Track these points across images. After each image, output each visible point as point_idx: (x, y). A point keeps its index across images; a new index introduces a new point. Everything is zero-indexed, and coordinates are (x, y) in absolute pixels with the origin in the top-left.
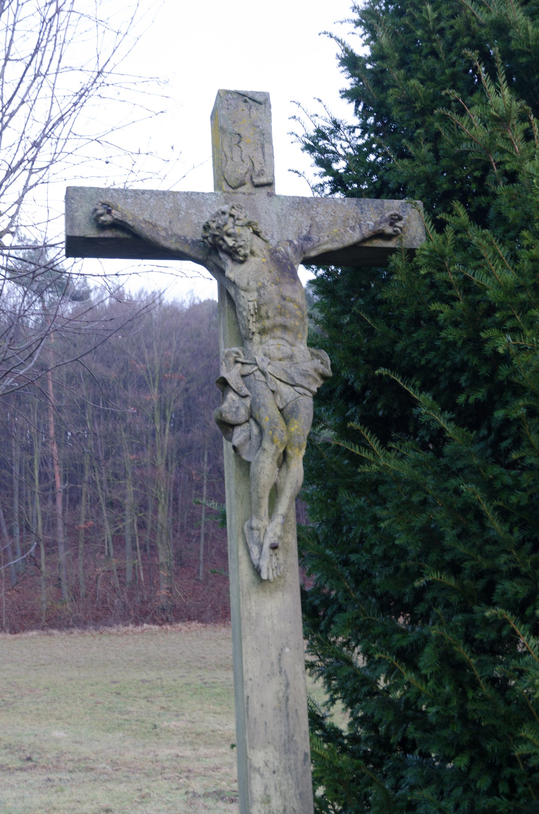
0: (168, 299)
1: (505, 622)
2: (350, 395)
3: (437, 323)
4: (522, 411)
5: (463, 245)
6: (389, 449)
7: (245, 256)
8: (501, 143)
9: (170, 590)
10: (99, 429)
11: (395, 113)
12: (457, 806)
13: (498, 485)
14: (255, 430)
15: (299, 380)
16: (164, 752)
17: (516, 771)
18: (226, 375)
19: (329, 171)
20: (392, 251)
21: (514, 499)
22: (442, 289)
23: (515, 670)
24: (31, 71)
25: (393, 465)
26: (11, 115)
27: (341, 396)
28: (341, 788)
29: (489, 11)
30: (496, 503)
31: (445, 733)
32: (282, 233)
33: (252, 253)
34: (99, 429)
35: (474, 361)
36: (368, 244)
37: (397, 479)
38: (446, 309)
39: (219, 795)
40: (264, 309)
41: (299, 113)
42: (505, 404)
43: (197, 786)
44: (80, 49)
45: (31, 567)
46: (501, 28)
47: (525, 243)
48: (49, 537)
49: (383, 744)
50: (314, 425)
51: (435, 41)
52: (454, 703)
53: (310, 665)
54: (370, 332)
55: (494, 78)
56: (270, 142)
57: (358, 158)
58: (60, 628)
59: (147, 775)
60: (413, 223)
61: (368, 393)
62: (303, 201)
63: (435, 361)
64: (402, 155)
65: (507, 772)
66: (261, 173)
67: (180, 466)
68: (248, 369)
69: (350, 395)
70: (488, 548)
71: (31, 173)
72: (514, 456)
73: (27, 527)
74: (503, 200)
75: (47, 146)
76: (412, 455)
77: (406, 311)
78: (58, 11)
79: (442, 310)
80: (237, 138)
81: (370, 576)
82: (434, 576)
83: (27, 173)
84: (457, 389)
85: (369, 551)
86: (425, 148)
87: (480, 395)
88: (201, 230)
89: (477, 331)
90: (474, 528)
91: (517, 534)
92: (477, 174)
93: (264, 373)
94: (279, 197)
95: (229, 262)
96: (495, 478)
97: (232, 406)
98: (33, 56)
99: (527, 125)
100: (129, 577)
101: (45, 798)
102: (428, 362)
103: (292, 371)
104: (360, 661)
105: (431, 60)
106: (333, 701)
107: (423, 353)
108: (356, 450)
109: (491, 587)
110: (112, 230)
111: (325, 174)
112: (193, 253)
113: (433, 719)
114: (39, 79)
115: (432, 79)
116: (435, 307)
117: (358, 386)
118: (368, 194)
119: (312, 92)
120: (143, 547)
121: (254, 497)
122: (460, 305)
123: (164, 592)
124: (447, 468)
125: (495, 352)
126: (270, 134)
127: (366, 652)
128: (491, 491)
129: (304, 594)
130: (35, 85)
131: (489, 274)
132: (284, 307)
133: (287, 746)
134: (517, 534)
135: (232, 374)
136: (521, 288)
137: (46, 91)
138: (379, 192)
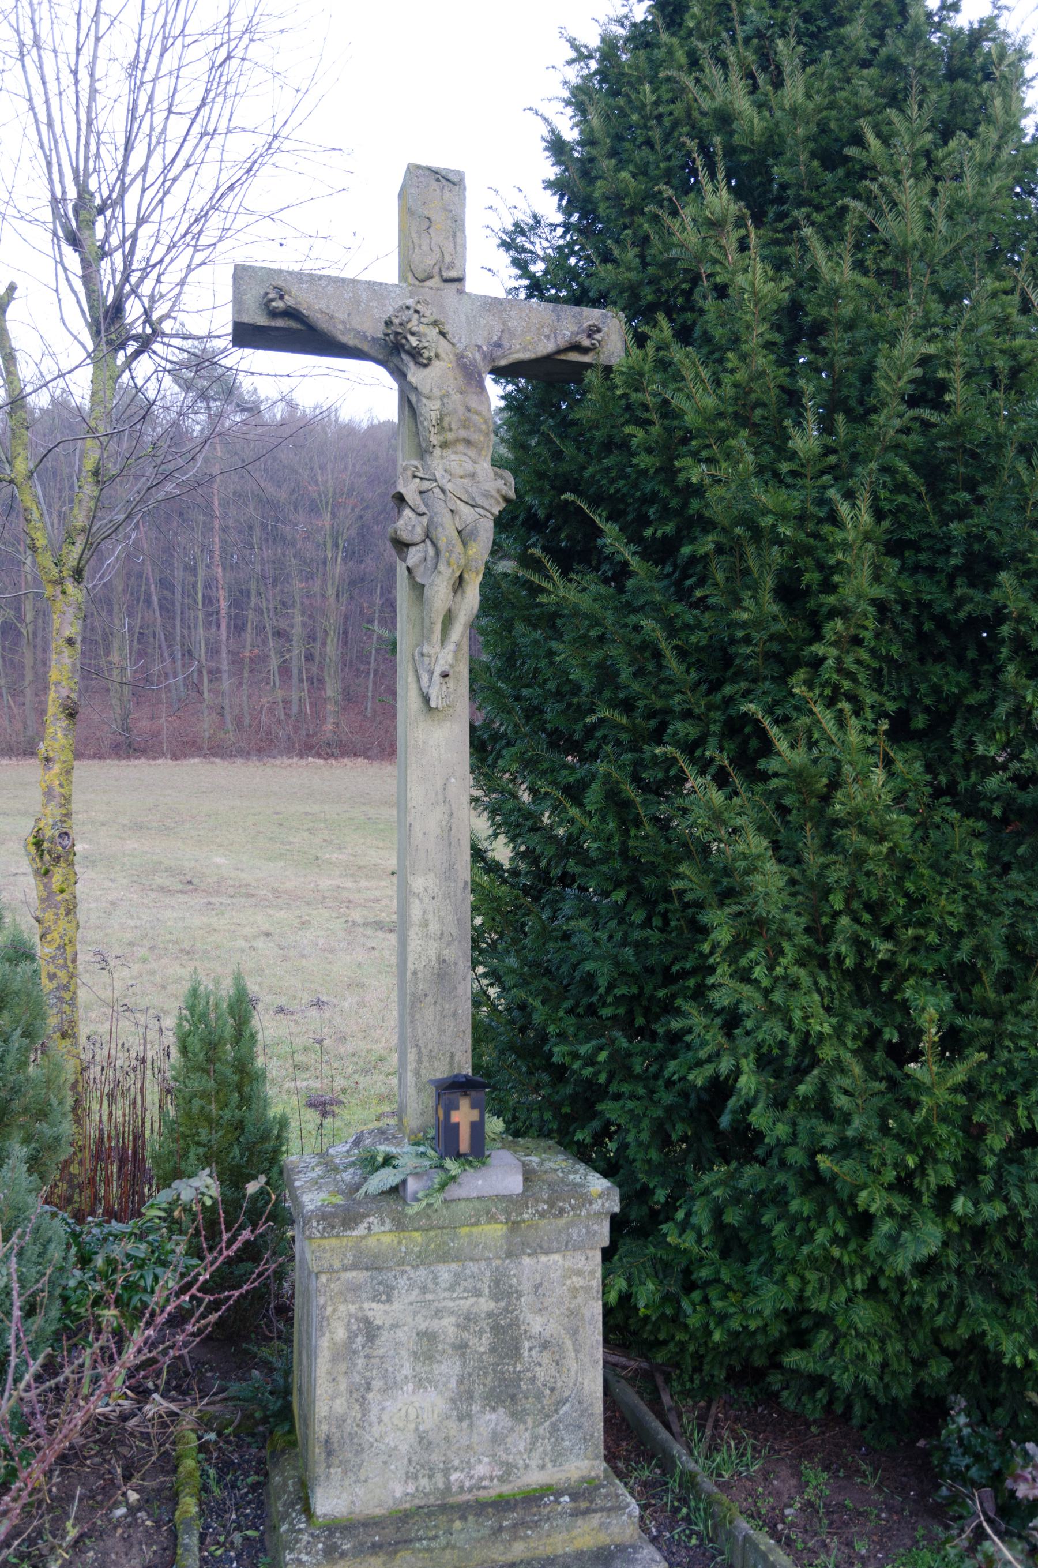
0: (345, 416)
1: (675, 760)
2: (533, 524)
3: (629, 448)
4: (712, 546)
5: (663, 365)
6: (570, 580)
7: (430, 359)
8: (713, 252)
9: (337, 725)
10: (267, 553)
11: (602, 210)
12: (611, 937)
13: (678, 623)
14: (431, 552)
15: (480, 500)
16: (325, 883)
17: (670, 906)
18: (403, 491)
19: (525, 273)
20: (588, 366)
21: (693, 639)
22: (638, 413)
23: (679, 809)
24: (197, 129)
25: (573, 596)
26: (175, 180)
27: (523, 524)
28: (498, 918)
29: (713, 98)
30: (675, 642)
31: (604, 868)
32: (472, 336)
33: (437, 356)
34: (267, 553)
35: (665, 492)
36: (562, 357)
37: (576, 613)
38: (639, 432)
39: (379, 925)
40: (447, 420)
41: (496, 202)
42: (693, 540)
43: (357, 915)
44: (254, 107)
45: (194, 694)
46: (725, 119)
47: (730, 365)
48: (213, 664)
49: (543, 878)
50: (493, 553)
51: (651, 128)
52: (616, 840)
53: (475, 800)
54: (558, 455)
55: (713, 176)
56: (463, 231)
57: (557, 263)
58: (222, 757)
59: (308, 904)
60: (611, 335)
61: (552, 522)
62: (496, 301)
63: (625, 490)
64: (607, 258)
65: (662, 907)
66: (451, 266)
67: (352, 598)
68: (426, 485)
69: (533, 524)
70: (663, 687)
71: (196, 251)
72: (698, 593)
73: (190, 652)
74: (710, 317)
75: (215, 220)
76: (593, 588)
77: (597, 434)
78: (229, 57)
79: (637, 434)
80: (427, 223)
81: (542, 712)
82: (606, 713)
83: (191, 249)
84: (644, 521)
85: (541, 686)
86: (632, 253)
87: (669, 528)
88: (382, 326)
89: (671, 460)
90: (651, 666)
91: (694, 675)
92: (685, 286)
93: (443, 491)
94: (469, 295)
95: (412, 364)
96: (677, 616)
97: (408, 524)
98: (199, 109)
99: (743, 232)
100: (295, 709)
101: (205, 920)
102: (618, 491)
103: (474, 490)
104: (526, 797)
105: (646, 150)
106: (496, 835)
107: (612, 481)
108: (535, 578)
109: (662, 728)
110: (283, 322)
111: (521, 277)
112: (372, 352)
113: (594, 855)
114: (207, 138)
115: (645, 173)
116: (629, 429)
117: (541, 513)
118: (566, 301)
119: (513, 185)
120: (310, 680)
121: (427, 620)
122: (655, 429)
123: (330, 727)
124: (628, 604)
125: (688, 484)
126: (463, 221)
127: (533, 791)
128: (671, 628)
129: (473, 728)
130: (202, 145)
131: (689, 397)
132: (468, 419)
133: (448, 873)
134: (694, 675)
135: (409, 490)
136: (721, 415)
137: (213, 154)
138: (580, 299)
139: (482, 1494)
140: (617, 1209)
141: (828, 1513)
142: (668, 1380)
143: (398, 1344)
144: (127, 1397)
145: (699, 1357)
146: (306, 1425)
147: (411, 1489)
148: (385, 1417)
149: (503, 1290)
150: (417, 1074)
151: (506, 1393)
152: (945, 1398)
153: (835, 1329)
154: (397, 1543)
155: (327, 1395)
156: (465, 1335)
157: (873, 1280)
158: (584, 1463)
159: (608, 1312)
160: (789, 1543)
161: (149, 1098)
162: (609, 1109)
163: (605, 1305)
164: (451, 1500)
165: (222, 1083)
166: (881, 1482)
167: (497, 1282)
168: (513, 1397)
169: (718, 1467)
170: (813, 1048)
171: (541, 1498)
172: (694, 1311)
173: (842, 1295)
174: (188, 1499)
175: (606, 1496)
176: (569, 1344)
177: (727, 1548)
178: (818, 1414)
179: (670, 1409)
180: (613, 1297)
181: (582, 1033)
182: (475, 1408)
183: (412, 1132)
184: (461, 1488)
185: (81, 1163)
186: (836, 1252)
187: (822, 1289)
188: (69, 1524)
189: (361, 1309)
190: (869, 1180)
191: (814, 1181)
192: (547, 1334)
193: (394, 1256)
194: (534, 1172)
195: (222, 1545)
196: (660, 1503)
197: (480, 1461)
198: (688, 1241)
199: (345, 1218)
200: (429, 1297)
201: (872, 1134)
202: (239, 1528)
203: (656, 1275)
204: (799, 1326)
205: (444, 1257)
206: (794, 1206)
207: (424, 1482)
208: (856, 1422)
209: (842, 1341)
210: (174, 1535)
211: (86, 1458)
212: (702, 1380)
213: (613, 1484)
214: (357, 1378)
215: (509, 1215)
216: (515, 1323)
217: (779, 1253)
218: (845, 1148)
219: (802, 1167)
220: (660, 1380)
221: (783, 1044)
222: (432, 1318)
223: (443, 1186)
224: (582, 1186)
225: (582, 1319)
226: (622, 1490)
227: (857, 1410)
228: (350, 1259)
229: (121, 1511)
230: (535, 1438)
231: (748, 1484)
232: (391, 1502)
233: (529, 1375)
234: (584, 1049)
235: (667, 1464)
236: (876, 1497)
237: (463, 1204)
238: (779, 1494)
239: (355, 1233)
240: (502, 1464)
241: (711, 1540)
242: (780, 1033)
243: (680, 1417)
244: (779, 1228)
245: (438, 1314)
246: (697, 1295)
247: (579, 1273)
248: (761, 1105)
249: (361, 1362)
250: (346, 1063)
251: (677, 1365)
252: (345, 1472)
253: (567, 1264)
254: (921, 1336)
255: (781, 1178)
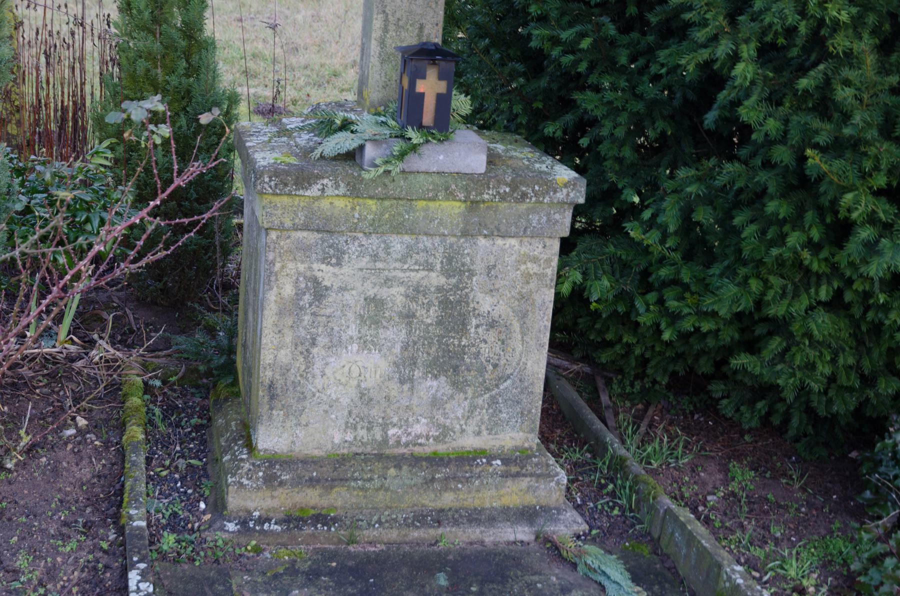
139: (417, 450)
140: (582, 201)
141: (749, 503)
142: (608, 382)
143: (345, 306)
144: (73, 343)
145: (644, 362)
146: (250, 375)
147: (349, 437)
148: (328, 371)
149: (454, 266)
150: (382, 43)
151: (450, 363)
152: (886, 418)
153: (791, 335)
154: (333, 480)
155: (272, 344)
156: (413, 306)
157: (838, 294)
158: (519, 434)
159: (560, 305)
160: (707, 522)
161: (88, 66)
162: (587, 101)
163: (557, 294)
164: (388, 452)
165: (170, 46)
166: (805, 484)
167: (450, 260)
168: (456, 369)
169: (648, 456)
170: (824, 40)
171: (474, 459)
172: (648, 310)
173: (805, 302)
174: (134, 427)
175: (536, 465)
176: (516, 326)
177: (647, 518)
178: (755, 423)
179: (607, 407)
180: (566, 288)
181: (566, 19)
182: (417, 374)
183: (372, 105)
184: (398, 443)
185: (19, 123)
186: (806, 255)
187: (783, 295)
188: (22, 432)
189: (310, 268)
190: (858, 183)
191: (801, 183)
192: (495, 314)
193: (347, 221)
194: (499, 156)
195: (169, 468)
196: (587, 480)
197: (418, 421)
198: (652, 238)
199: (298, 177)
200: (380, 265)
201: (872, 134)
202: (183, 456)
203: (613, 274)
204: (753, 328)
205: (398, 228)
206: (771, 206)
207: (362, 433)
208: (791, 433)
209: (794, 349)
210: (122, 455)
211: (35, 388)
212: (643, 387)
213: (545, 456)
214: (303, 333)
215: (469, 193)
216: (464, 300)
217: (746, 253)
218: (836, 148)
219: (787, 166)
220: (600, 383)
221: (791, 31)
222: (381, 286)
223: (402, 155)
224: (549, 174)
225: (533, 304)
226: (552, 461)
227: (795, 422)
228: (301, 218)
229: (71, 432)
230: (473, 408)
231: (676, 473)
232: (329, 446)
233: (473, 350)
234: (566, 35)
235: (598, 448)
236: (799, 495)
237: (421, 177)
238: (704, 484)
239: (308, 193)
240: (439, 426)
241: (631, 511)
242: (792, 18)
243: (616, 414)
244: (750, 230)
245: (388, 282)
246: (652, 297)
247: (535, 260)
248: (754, 98)
249: (307, 318)
250: (298, 74)
251: (620, 371)
252: (287, 415)
253: (524, 250)
254: (876, 354)
255: (762, 177)
